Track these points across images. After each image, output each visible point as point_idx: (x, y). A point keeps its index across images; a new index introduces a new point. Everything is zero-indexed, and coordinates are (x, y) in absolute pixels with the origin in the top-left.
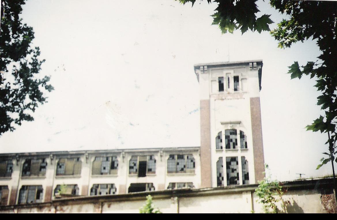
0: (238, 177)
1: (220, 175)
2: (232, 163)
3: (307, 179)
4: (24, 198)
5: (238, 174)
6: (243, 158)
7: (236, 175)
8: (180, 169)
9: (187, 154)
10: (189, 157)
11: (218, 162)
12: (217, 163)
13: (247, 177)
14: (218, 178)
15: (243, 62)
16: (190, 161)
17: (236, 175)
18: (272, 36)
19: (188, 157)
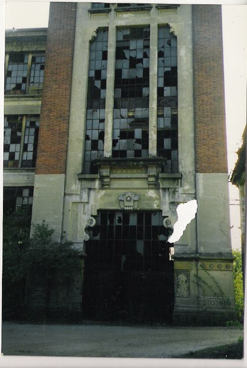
0: (145, 81)
1: (98, 74)
2: (133, 45)
3: (181, 181)
4: (200, 184)
5: (146, 71)
6: (164, 27)
7: (140, 74)
8: (14, 86)
9: (32, 52)
10: (38, 60)
11: (93, 41)
12: (91, 42)
13: (167, 6)
14: (91, 81)
15: (192, 58)
16: (38, 67)
17: (140, 74)
18: (168, 217)
19: (34, 59)
